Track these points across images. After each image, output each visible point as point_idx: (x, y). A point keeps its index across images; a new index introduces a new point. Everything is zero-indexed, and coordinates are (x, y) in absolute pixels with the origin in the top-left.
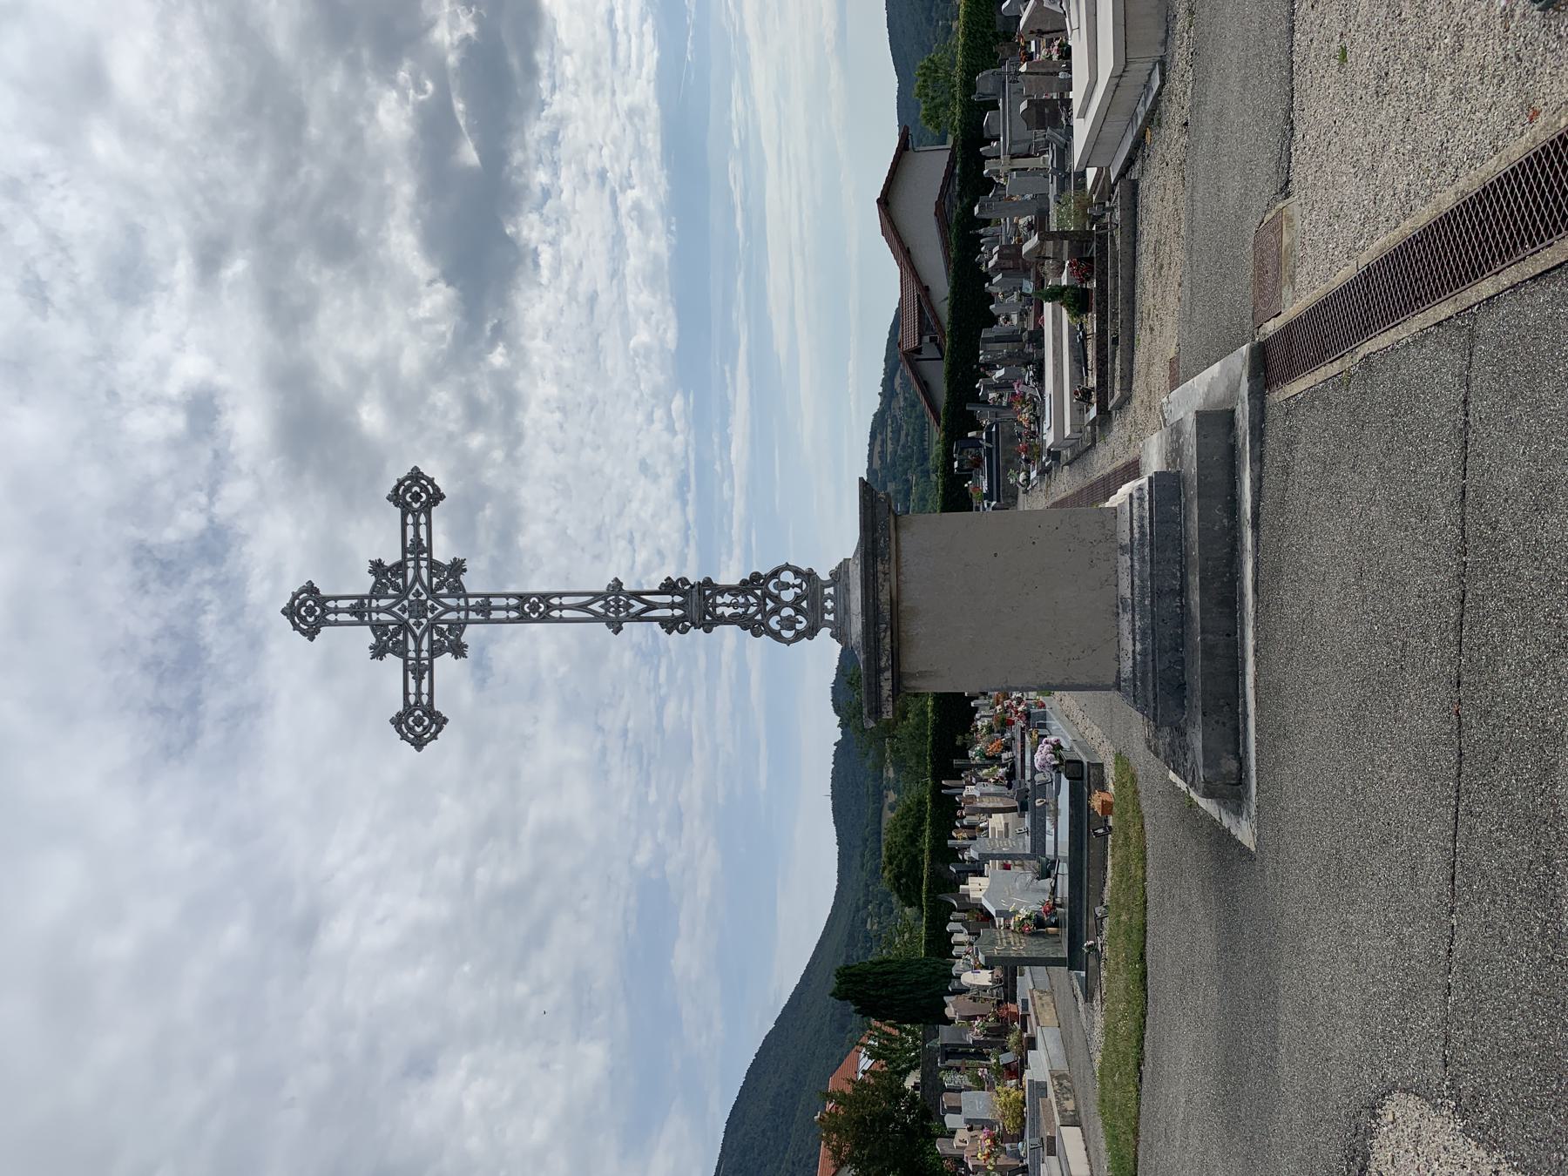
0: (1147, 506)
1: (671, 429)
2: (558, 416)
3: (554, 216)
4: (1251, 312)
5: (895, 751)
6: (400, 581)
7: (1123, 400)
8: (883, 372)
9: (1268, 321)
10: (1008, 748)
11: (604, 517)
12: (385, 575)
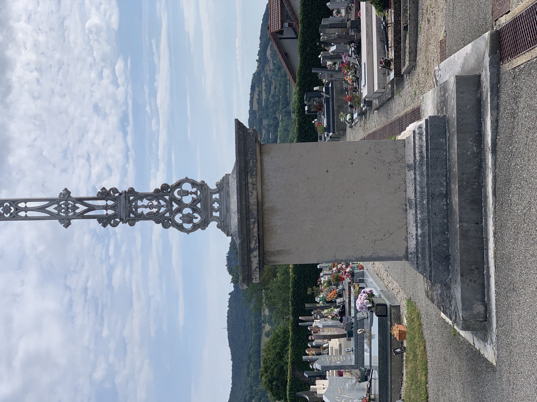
1: (115, 83)
2: (35, 74)
4: (491, 10)
5: (269, 298)
7: (410, 67)
9: (502, 16)
10: (340, 296)
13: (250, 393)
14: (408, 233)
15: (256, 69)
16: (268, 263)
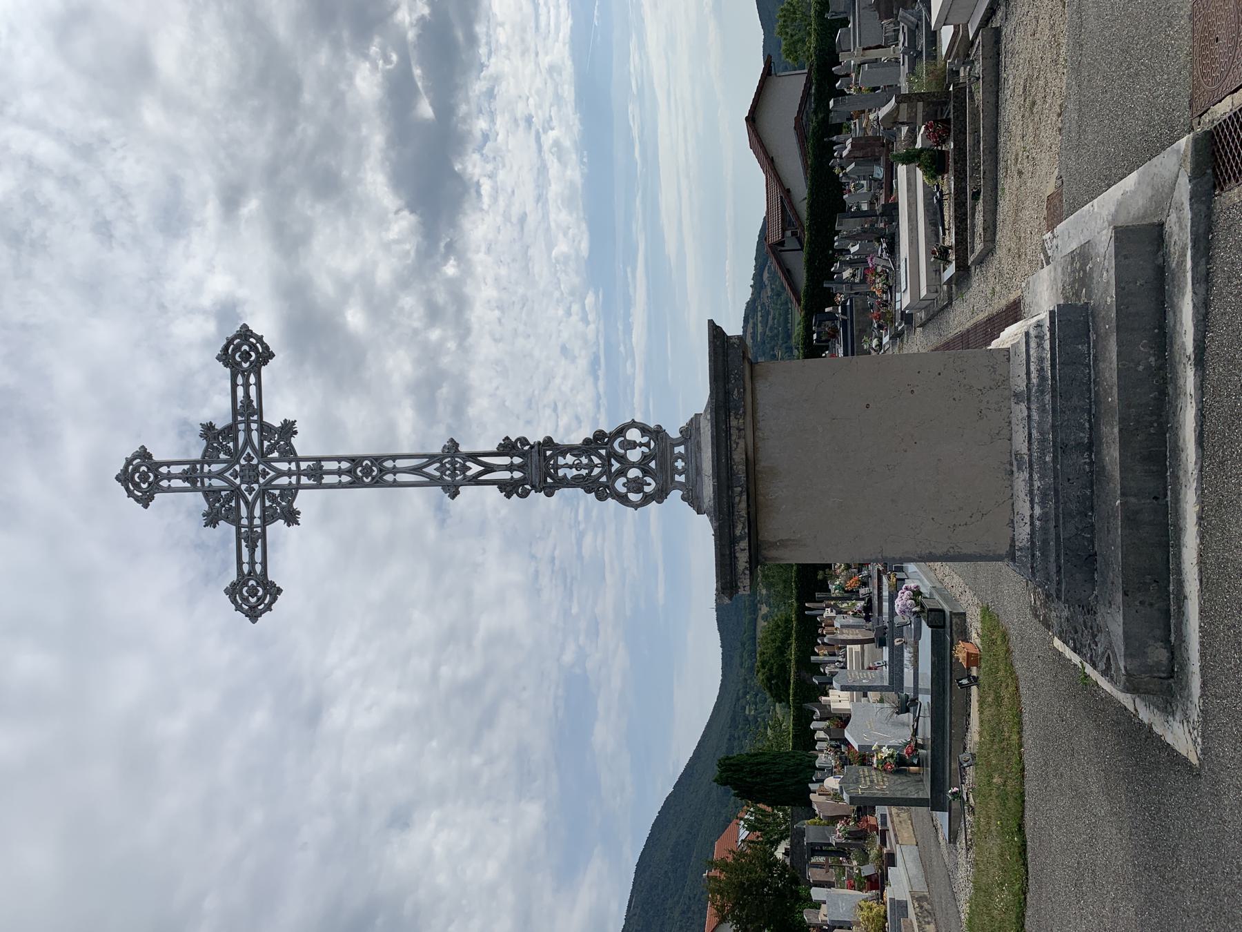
0: (1047, 345)
1: (585, 320)
2: (497, 313)
3: (491, 155)
5: (765, 576)
6: (231, 445)
8: (754, 268)
9: (1220, 101)
10: (865, 584)
11: (533, 391)
12: (216, 438)
13: (744, 687)
14: (1016, 514)
15: (750, 296)
16: (766, 560)
